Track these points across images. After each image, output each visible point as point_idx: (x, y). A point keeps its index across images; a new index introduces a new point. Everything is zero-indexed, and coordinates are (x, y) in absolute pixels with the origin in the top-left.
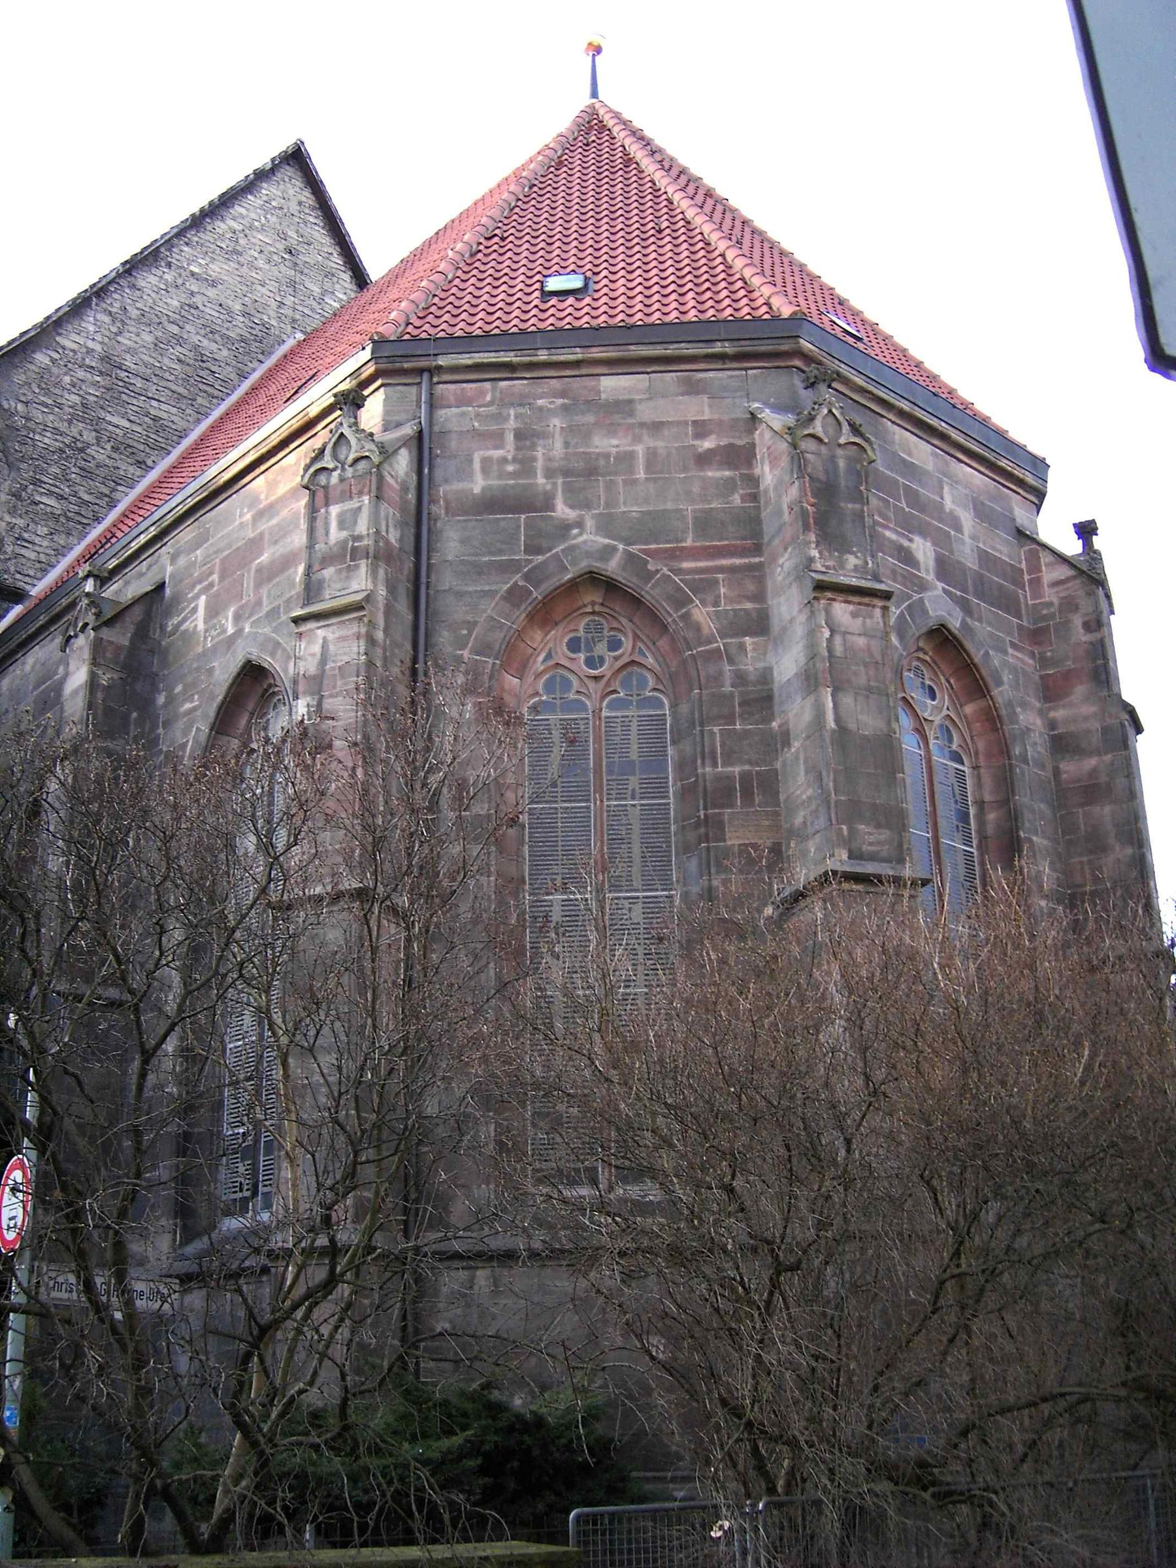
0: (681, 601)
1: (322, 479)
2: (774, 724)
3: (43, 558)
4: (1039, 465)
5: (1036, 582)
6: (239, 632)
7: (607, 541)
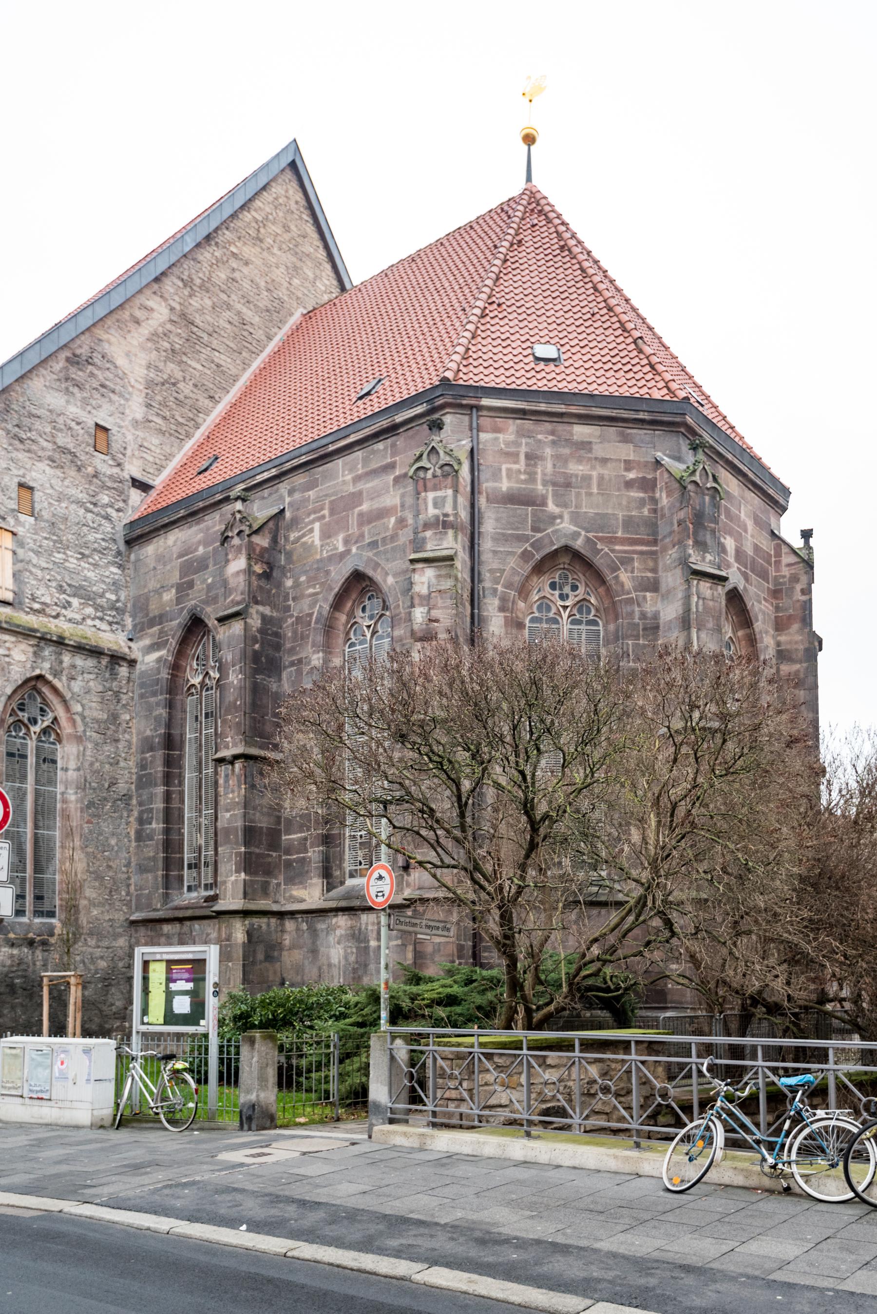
0: (615, 569)
3: (158, 461)
4: (786, 492)
5: (778, 563)
6: (348, 551)
7: (576, 529)
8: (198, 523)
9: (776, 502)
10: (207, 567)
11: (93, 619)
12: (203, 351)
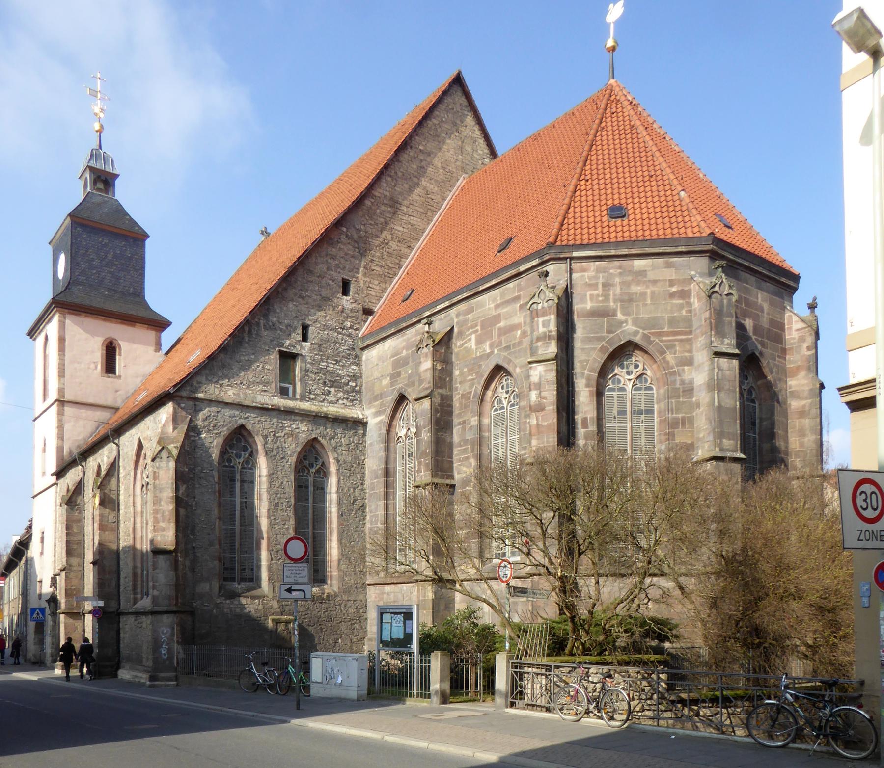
0: (663, 353)
1: (535, 306)
2: (694, 399)
3: (378, 294)
6: (492, 352)
7: (636, 329)
8: (402, 336)
9: (788, 286)
10: (408, 363)
11: (343, 400)
12: (404, 218)
